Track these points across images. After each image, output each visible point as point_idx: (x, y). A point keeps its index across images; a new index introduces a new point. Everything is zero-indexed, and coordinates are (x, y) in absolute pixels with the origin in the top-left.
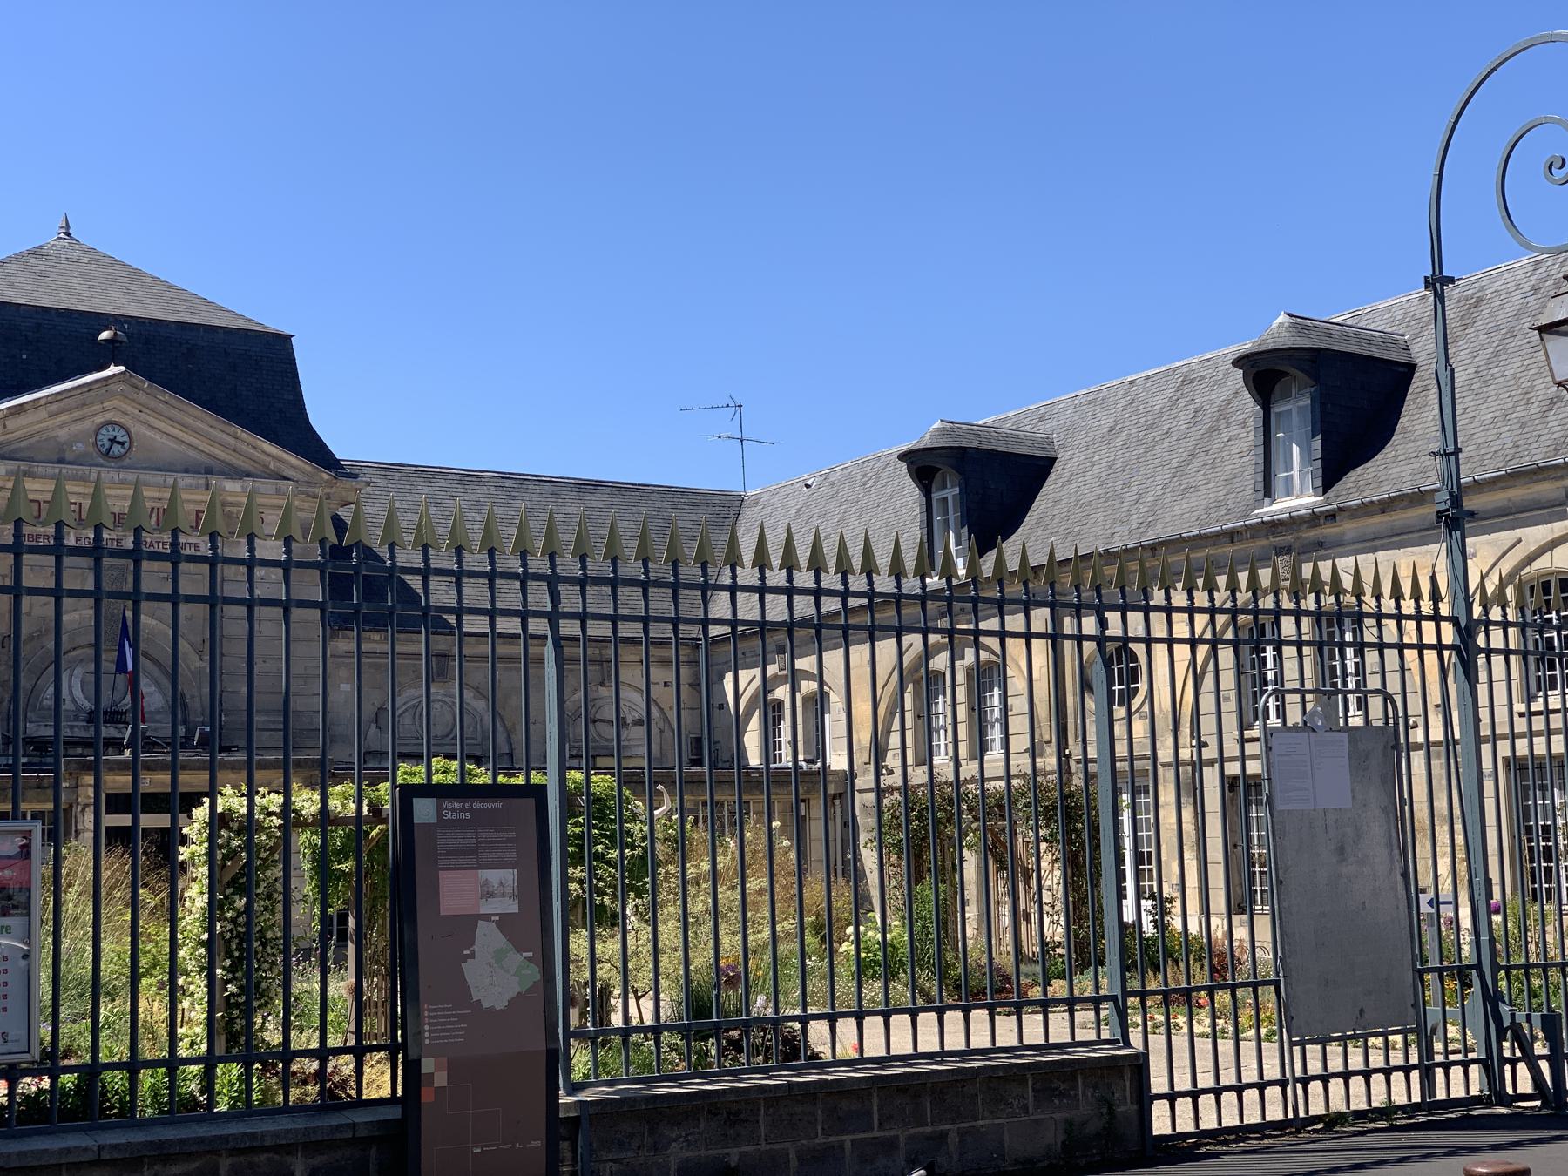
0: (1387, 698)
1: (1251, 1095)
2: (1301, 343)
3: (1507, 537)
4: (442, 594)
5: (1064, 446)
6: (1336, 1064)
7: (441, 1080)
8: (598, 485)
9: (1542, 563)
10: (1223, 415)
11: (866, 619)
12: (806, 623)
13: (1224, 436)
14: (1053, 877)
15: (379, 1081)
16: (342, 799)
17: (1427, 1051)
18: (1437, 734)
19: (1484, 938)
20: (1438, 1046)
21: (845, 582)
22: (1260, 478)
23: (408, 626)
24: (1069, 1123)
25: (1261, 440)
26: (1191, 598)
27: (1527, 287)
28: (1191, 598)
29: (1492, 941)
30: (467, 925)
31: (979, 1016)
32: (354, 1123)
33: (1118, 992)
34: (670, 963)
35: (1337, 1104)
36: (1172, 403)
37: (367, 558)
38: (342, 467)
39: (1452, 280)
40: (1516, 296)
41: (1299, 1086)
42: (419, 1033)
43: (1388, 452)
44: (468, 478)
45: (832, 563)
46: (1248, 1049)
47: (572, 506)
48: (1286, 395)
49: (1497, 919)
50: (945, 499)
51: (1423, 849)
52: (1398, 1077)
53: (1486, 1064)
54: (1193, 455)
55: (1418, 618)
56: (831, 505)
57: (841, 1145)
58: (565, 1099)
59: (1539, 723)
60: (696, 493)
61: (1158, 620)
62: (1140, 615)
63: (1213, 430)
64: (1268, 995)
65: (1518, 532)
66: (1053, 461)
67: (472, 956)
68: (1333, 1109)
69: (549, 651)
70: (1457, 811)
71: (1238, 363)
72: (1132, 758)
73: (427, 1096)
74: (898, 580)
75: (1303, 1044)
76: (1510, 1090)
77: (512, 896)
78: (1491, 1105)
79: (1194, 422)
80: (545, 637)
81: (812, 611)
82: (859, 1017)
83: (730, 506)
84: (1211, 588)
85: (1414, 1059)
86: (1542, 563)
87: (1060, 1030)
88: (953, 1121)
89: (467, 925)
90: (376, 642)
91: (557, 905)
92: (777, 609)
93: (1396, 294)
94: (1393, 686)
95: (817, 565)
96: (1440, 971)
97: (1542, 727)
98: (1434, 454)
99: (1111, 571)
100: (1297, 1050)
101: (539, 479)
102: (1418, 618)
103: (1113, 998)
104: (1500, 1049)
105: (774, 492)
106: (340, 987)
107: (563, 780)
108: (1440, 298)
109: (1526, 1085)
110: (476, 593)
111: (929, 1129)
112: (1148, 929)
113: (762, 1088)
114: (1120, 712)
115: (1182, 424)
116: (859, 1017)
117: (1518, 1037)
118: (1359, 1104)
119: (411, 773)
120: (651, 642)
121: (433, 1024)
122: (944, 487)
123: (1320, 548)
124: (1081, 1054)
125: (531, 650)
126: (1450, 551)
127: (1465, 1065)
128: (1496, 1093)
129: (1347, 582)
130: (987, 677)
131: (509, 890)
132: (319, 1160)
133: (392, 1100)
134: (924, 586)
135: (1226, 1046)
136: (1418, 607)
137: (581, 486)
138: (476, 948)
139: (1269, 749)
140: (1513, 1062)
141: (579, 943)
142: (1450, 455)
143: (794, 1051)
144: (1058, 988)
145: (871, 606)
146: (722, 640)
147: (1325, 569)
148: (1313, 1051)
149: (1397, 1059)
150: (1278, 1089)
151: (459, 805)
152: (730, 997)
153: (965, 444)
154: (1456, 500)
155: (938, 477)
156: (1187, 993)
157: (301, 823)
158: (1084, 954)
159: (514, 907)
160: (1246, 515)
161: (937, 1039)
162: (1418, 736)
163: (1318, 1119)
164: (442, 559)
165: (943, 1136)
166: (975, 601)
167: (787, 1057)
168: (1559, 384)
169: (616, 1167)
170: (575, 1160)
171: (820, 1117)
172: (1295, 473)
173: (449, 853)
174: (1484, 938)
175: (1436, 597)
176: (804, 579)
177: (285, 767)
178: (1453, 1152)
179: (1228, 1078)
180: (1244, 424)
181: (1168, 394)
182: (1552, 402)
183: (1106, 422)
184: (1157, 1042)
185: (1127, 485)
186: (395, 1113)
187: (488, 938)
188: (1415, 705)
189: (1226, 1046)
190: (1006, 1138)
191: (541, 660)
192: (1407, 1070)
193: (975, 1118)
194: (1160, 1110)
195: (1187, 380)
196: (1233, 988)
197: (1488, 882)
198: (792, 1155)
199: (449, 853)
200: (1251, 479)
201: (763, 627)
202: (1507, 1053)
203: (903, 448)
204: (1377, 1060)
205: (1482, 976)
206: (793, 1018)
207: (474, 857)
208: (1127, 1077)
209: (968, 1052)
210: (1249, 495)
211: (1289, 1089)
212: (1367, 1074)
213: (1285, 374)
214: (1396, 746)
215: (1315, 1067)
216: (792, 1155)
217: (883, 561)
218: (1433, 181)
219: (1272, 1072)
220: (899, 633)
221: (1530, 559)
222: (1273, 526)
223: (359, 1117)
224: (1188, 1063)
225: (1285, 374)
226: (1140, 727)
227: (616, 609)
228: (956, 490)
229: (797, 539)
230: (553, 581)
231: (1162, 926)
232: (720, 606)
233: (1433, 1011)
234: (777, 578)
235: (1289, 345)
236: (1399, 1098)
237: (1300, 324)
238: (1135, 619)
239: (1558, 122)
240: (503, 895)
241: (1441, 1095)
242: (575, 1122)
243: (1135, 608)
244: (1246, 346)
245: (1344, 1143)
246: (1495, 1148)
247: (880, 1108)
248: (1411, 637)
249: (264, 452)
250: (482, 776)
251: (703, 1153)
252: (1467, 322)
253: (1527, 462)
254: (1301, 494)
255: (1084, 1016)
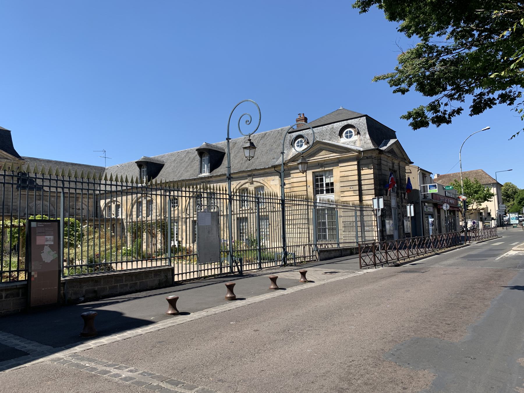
0: (217, 207)
1: (192, 274)
2: (207, 148)
3: (238, 182)
4: (39, 182)
5: (166, 162)
6: (206, 268)
7: (36, 276)
8: (76, 164)
9: (244, 186)
10: (194, 159)
11: (131, 191)
12: (119, 191)
13: (194, 163)
14: (159, 236)
15: (22, 276)
16: (15, 223)
17: (221, 265)
18: (225, 213)
19: (231, 246)
20: (223, 264)
21: (122, 184)
22: (200, 170)
23: (31, 189)
24: (160, 280)
25: (200, 164)
26: (186, 189)
27: (243, 142)
28: (186, 189)
29: (232, 247)
30: (42, 247)
31: (144, 262)
32: (17, 285)
33: (170, 257)
34: (85, 254)
35: (206, 274)
36: (185, 156)
37: (22, 175)
38: (21, 158)
39: (230, 139)
40: (241, 143)
41: (200, 272)
42: (31, 267)
43: (221, 167)
44: (49, 161)
45: (120, 180)
46: (192, 266)
47: (70, 167)
48: (204, 156)
49: (233, 243)
50: (144, 171)
51: (222, 232)
52: (216, 270)
53: (230, 267)
54: (189, 165)
55: (223, 194)
56: (122, 170)
57: (117, 286)
58: (62, 279)
59: (244, 212)
60: (96, 167)
61: (184, 193)
62: (177, 192)
63: (192, 161)
64: (195, 257)
65: (240, 181)
66: (164, 165)
67: (43, 252)
68: (205, 275)
69: (62, 194)
70: (228, 226)
71: (197, 150)
72: (174, 217)
73: (32, 279)
74: (132, 184)
75: (201, 265)
76: (234, 271)
77: (52, 241)
78: (231, 273)
79: (189, 160)
80: (61, 192)
81: (121, 189)
82: (122, 263)
83: (103, 169)
84: (189, 188)
85: (219, 266)
86: (244, 186)
87: (159, 263)
88: (138, 280)
89: (42, 247)
90: (25, 192)
91: (62, 243)
92: (114, 188)
93: (223, 141)
94: (219, 205)
95: (117, 180)
96: (224, 252)
97: (241, 213)
98: (227, 167)
99: (172, 185)
100: (200, 265)
101: (64, 163)
102: (223, 194)
103: (169, 258)
104: (233, 264)
105: (111, 168)
106: (15, 259)
107: (64, 219)
108: (228, 141)
109: (236, 270)
110: (47, 183)
111: (134, 282)
112: (177, 246)
113: (114, 274)
114: (172, 209)
115: (187, 160)
116: (122, 263)
117: (236, 262)
118: (210, 274)
119: (31, 218)
120: (89, 194)
121: (34, 265)
122: (144, 168)
123: (209, 182)
124: (163, 268)
125: (58, 195)
126: (228, 184)
127: (227, 267)
128: (232, 271)
129: (212, 187)
130: (150, 203)
131: (51, 240)
132: (8, 292)
133: (25, 280)
134: (210, 191)
135: (188, 266)
136: (223, 192)
137: (73, 164)
138: (44, 251)
139: (198, 215)
140: (235, 266)
141: (66, 250)
142: (229, 167)
143: (110, 269)
144: (160, 257)
145: (132, 189)
146: (103, 194)
147: (208, 186)
148: (203, 266)
149: (216, 266)
150: (196, 272)
151: (41, 223)
152: (97, 260)
153: (148, 161)
154: (230, 175)
155: (143, 166)
156: (182, 257)
157: (7, 227)
158: (166, 251)
159: (52, 243)
160: (197, 176)
161: (136, 266)
162: (222, 214)
163: (203, 277)
164: (39, 176)
165: (137, 283)
166: (151, 189)
167: (108, 270)
168: (246, 157)
169: (73, 291)
170: (64, 290)
171: (113, 280)
172: (206, 169)
173: (39, 233)
174: (231, 246)
175: (226, 191)
176: (221, 192)
177: (11, 216)
178: (224, 281)
179: (188, 271)
180: (197, 161)
181: (185, 155)
182: (246, 160)
183: (174, 158)
184: (176, 265)
185: (177, 170)
186: (26, 283)
187: (47, 249)
188: (222, 209)
189: (188, 266)
190: (148, 283)
191: (60, 197)
192: (218, 268)
193: (143, 280)
194: (176, 277)
195: (188, 152)
196: (190, 256)
197: (232, 237)
198: (108, 288)
199: (39, 233)
200: (198, 170)
201: (111, 192)
202: (234, 265)
203: (136, 161)
204: (213, 267)
205: (230, 252)
206: (109, 263)
207: (44, 234)
208: (171, 271)
209: (142, 268)
210: (198, 173)
211: (198, 272)
212: (211, 269)
213: (204, 153)
214: (219, 215)
215: (203, 268)
216: (108, 288)
217: (130, 180)
218: (228, 122)
219: (196, 270)
220: (137, 194)
221: (242, 185)
222: (202, 178)
223: (18, 284)
224: (181, 269)
225: (204, 153)
226: (176, 212)
227: (76, 187)
228: (146, 169)
229: (128, 178)
230: (63, 181)
231: (179, 246)
232: (103, 187)
233: (222, 259)
234: (109, 182)
235: (205, 148)
236: (216, 273)
237: (207, 144)
238: (176, 192)
239: (248, 114)
240: (50, 241)
241: (223, 272)
242: (64, 283)
243: (176, 191)
244: (198, 148)
245: (207, 281)
246: (231, 280)
247: (125, 279)
248: (188, 195)
249: (4, 154)
250: (47, 218)
251: (90, 288)
252: (234, 146)
253: (242, 170)
254: (206, 173)
255: (164, 262)
